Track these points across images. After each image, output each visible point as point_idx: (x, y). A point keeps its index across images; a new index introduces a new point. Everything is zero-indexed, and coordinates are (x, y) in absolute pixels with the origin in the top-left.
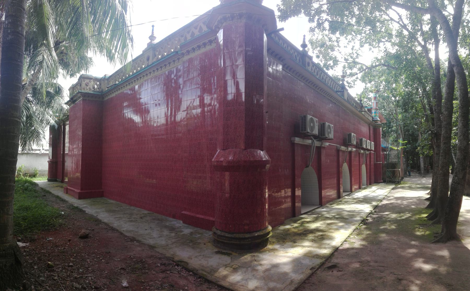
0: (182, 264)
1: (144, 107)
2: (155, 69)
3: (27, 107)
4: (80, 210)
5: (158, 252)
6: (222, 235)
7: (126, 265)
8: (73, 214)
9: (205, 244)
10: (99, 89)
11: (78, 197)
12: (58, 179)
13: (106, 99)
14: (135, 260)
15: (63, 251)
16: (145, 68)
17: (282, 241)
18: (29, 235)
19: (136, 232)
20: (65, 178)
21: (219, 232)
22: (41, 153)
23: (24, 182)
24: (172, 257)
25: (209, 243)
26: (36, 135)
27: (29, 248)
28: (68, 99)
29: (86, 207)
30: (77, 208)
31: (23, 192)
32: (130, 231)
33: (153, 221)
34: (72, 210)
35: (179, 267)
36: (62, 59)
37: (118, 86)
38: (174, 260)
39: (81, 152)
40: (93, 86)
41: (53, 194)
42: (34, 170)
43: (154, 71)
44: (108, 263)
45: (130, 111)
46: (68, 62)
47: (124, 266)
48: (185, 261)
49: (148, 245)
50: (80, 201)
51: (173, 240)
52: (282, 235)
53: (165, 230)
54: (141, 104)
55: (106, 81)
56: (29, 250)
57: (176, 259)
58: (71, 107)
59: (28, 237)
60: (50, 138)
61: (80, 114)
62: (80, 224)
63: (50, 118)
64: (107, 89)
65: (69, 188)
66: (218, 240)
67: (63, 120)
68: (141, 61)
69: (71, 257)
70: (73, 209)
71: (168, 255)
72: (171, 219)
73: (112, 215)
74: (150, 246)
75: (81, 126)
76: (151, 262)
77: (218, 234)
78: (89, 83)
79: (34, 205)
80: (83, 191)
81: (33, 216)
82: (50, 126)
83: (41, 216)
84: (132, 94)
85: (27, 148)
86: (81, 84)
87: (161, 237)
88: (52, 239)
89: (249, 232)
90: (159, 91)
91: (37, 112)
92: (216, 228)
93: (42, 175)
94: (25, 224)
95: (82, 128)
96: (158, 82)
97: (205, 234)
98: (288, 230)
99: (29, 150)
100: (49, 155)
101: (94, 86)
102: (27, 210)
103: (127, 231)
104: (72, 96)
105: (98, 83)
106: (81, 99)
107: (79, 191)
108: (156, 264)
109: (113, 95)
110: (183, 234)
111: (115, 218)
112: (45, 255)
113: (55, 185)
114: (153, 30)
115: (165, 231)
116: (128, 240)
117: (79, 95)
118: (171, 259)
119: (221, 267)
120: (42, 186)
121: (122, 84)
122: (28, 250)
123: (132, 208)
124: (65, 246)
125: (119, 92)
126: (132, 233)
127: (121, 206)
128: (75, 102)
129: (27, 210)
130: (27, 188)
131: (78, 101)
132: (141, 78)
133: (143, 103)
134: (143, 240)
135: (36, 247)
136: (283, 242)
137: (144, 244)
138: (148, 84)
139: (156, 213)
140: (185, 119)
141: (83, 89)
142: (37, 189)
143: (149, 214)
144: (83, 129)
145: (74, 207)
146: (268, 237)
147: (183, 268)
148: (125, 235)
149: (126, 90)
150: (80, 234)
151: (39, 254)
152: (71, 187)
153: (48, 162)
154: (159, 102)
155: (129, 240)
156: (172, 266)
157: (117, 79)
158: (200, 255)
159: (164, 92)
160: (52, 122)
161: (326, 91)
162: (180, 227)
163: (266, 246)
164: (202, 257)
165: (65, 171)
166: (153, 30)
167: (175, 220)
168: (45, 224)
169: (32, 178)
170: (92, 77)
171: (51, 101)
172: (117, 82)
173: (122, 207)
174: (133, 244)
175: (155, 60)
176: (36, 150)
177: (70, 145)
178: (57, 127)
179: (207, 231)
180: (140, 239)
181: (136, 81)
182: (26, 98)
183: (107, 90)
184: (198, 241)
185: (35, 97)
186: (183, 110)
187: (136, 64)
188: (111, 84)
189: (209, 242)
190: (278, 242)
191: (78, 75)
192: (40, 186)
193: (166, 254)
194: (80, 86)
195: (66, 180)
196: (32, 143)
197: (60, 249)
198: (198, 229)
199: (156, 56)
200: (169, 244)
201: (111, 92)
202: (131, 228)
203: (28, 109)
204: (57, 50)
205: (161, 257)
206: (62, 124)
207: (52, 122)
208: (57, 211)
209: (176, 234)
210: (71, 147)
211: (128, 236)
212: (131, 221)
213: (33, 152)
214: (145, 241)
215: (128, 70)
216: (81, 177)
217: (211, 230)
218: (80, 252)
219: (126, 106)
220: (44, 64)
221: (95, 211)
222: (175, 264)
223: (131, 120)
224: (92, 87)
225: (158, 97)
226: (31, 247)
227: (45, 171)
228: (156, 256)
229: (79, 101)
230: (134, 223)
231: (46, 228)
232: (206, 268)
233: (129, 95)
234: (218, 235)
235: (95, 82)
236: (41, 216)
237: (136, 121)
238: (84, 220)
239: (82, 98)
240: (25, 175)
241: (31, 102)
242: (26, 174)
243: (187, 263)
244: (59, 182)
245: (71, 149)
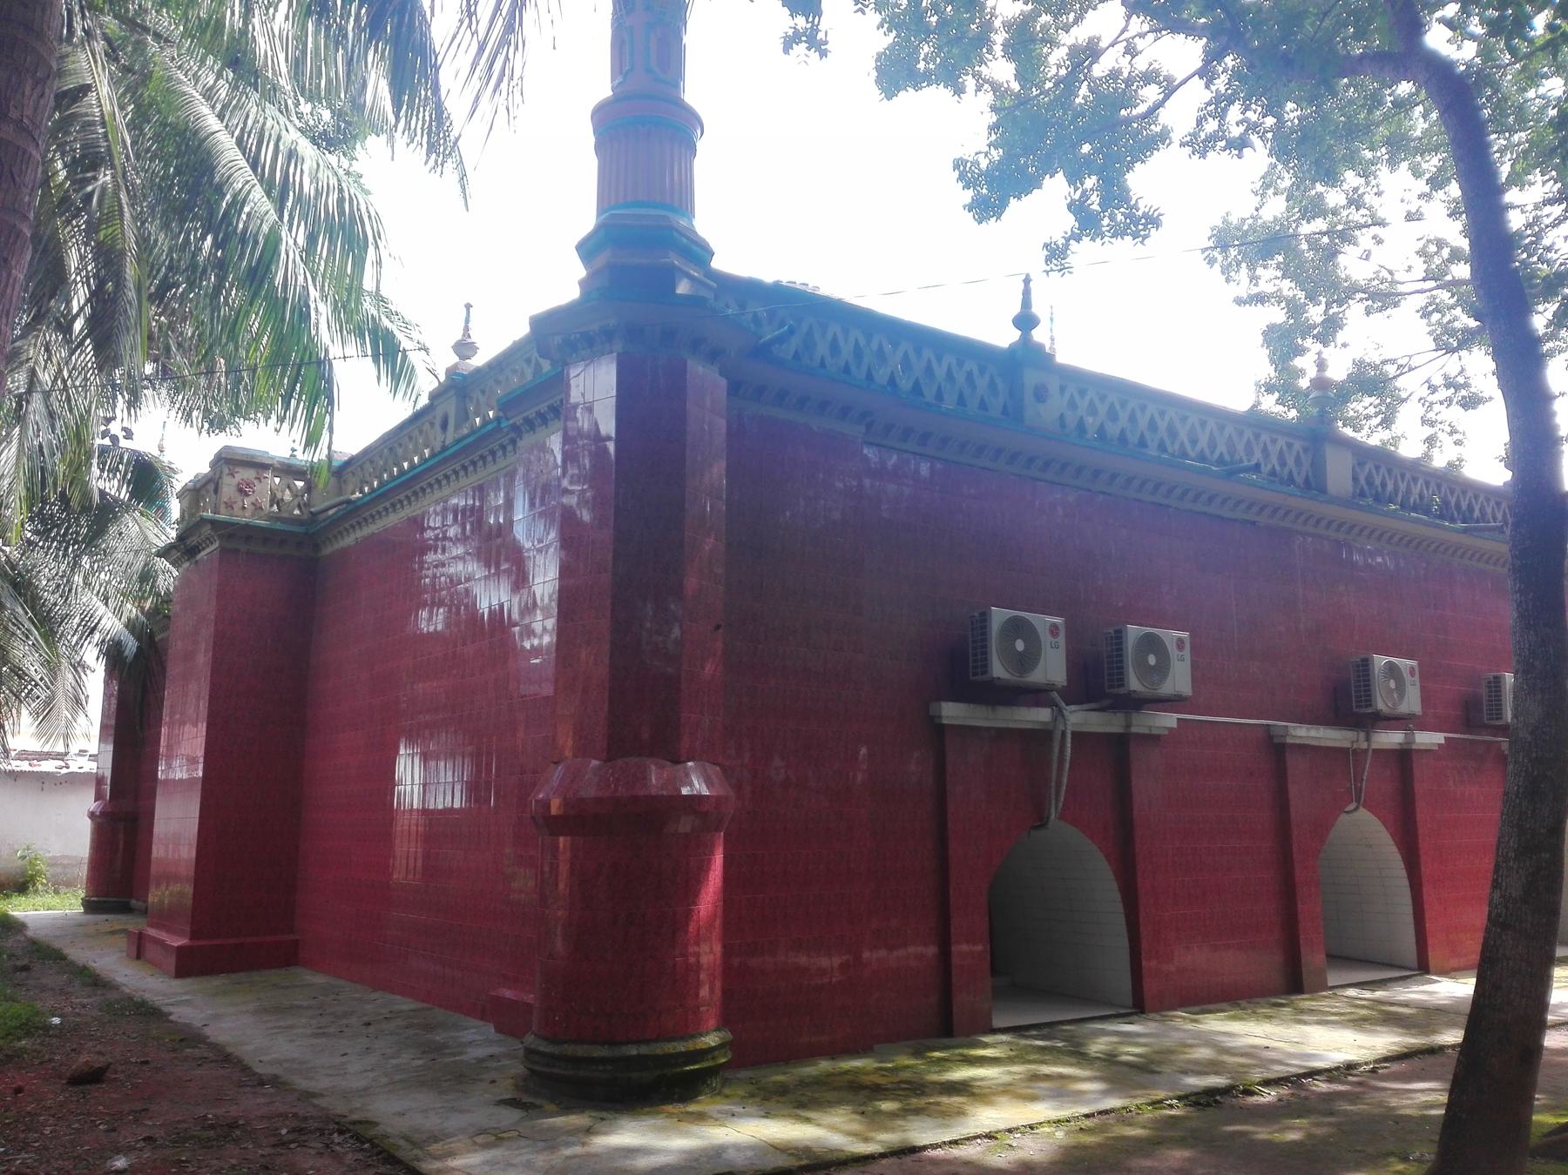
11: (172, 969)
12: (133, 902)
13: (327, 550)
22: (64, 771)
28: (1200, 64)
37: (357, 509)
41: (72, 963)
42: (23, 858)
63: (102, 609)
65: (152, 932)
78: (256, 482)
89: (612, 1043)
93: (59, 885)
109: (349, 540)
114: (467, 321)
128: (196, 554)
141: (223, 506)
153: (92, 815)
161: (1365, 527)
166: (467, 321)
239: (216, 545)
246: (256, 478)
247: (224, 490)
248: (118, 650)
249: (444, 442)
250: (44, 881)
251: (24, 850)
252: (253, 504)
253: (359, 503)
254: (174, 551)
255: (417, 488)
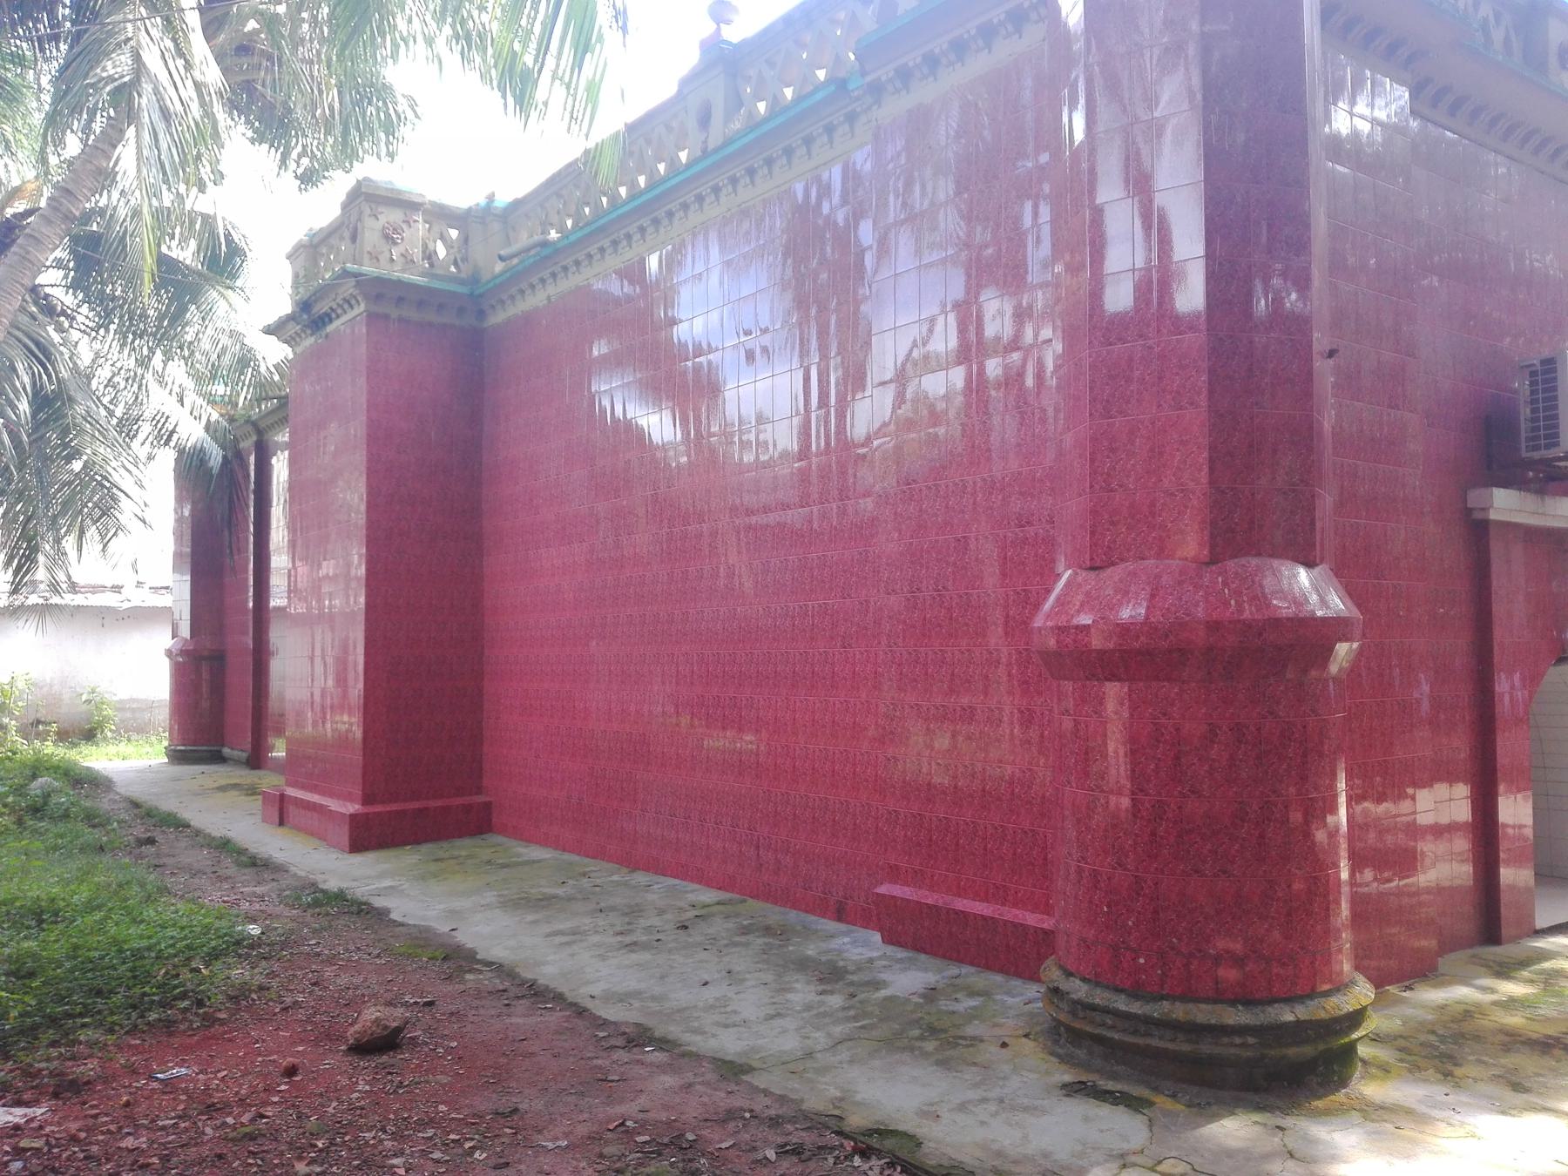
0: (889, 1143)
1: (689, 363)
2: (739, 171)
3: (37, 344)
4: (355, 908)
5: (766, 1092)
6: (1097, 1001)
7: (599, 1167)
8: (315, 931)
9: (1004, 1045)
10: (456, 263)
11: (345, 840)
12: (226, 751)
13: (497, 318)
14: (647, 1138)
15: (247, 1130)
16: (689, 166)
17: (1438, 1070)
18: (48, 1060)
19: (653, 998)
20: (271, 740)
21: (1079, 989)
23: (28, 772)
24: (836, 1112)
25: (1024, 1039)
26: (96, 505)
27: (48, 1129)
28: (286, 308)
29: (391, 887)
30: (340, 896)
31: (20, 822)
32: (624, 998)
33: (743, 939)
34: (310, 911)
35: (875, 1162)
36: (248, 81)
38: (847, 1129)
39: (362, 600)
40: (425, 246)
41: (198, 833)
42: (88, 701)
43: (734, 181)
44: (507, 1164)
45: (622, 386)
46: (285, 103)
47: (591, 1170)
48: (901, 1128)
49: (714, 1060)
50: (357, 859)
51: (838, 1030)
52: (1432, 1038)
53: (797, 981)
54: (678, 353)
55: (496, 226)
56: (47, 1143)
57: (856, 1121)
58: (299, 350)
59: (41, 1070)
60: (179, 520)
61: (354, 392)
62: (357, 980)
64: (499, 267)
65: (291, 792)
66: (1077, 1025)
67: (254, 424)
68: (669, 128)
69: (300, 1158)
70: (316, 903)
71: (814, 1103)
72: (831, 925)
73: (535, 922)
74: (725, 1062)
75: (360, 458)
76: (723, 1146)
77: (1074, 996)
79: (83, 894)
80: (379, 808)
81: (75, 958)
82: (181, 451)
83: (121, 951)
84: (629, 299)
85: (41, 574)
86: (356, 229)
87: (778, 1015)
88: (184, 1071)
89: (1249, 1002)
90: (763, 284)
91: (104, 373)
92: (1061, 967)
93: (133, 728)
94: (26, 999)
95: (363, 469)
96: (758, 238)
97: (1006, 998)
98: (1469, 1013)
99: (54, 587)
100: (177, 616)
101: (431, 246)
102: (41, 922)
103: (610, 997)
104: (304, 293)
105: (454, 233)
106: (356, 311)
107: (353, 808)
108: (754, 1149)
110: (886, 999)
111: (548, 935)
112: (142, 1160)
113: (210, 783)
115: (798, 986)
116: (613, 1042)
117: (348, 288)
118: (831, 1123)
119: (1098, 1164)
120: (136, 792)
121: (580, 241)
122: (37, 1144)
123: (641, 878)
124: (266, 1103)
125: (566, 284)
126: (637, 1004)
127: (584, 875)
128: (324, 325)
129: (41, 922)
130: (46, 804)
131: (344, 318)
132: (670, 214)
133: (686, 344)
134: (687, 1037)
135: (91, 1122)
136: (1446, 1075)
137: (697, 1057)
138: (707, 248)
139: (755, 896)
140: (892, 427)
141: (366, 257)
142: (104, 804)
143: (721, 908)
144: (371, 473)
145: (324, 892)
146: (1355, 1036)
147: (891, 1165)
148: (600, 1017)
149: (604, 278)
150: (352, 1030)
151: (108, 1160)
152: (303, 787)
153: (169, 653)
154: (766, 340)
155: (620, 1042)
156: (837, 1158)
157: (555, 219)
158: (984, 1100)
159: (783, 290)
160: (192, 432)
162: (871, 961)
163: (1343, 1082)
164: (994, 1108)
165: (273, 704)
167: (842, 927)
168: (144, 994)
169: (74, 745)
170: (419, 200)
171: (183, 310)
172: (554, 235)
173: (586, 880)
174: (640, 1062)
175: (736, 125)
176: (96, 589)
177: (298, 563)
178: (220, 459)
179: (1016, 983)
180: (673, 1031)
181: (650, 230)
182: (34, 290)
183: (503, 272)
184: (970, 1030)
185: (86, 290)
186: (876, 381)
187: (649, 142)
188: (524, 239)
189: (1026, 1036)
190: (1410, 1071)
191: (338, 186)
192: (122, 791)
193: (802, 1101)
194: (354, 238)
195: (279, 752)
196: (69, 543)
197: (230, 1120)
198: (966, 969)
199: (741, 104)
200: (819, 1047)
201: (524, 285)
202: (632, 983)
203: (42, 354)
204: (219, 29)
205: (778, 1116)
206: (247, 444)
207: (192, 432)
208: (217, 924)
209: (853, 996)
210: (302, 569)
211: (615, 1023)
212: (633, 946)
213: (79, 600)
214: (698, 1038)
215: (605, 169)
216: (365, 732)
217: (1034, 977)
218: (350, 1123)
219: (604, 359)
220: (144, 101)
221: (442, 906)
222: (849, 1145)
223: (633, 435)
224: (417, 253)
225: (756, 315)
226: (59, 1124)
227: (151, 706)
228: (751, 1111)
229: (349, 322)
230: (644, 956)
231: (153, 1016)
232: (1015, 1162)
233: (617, 302)
234: (1078, 1002)
235: (436, 228)
236: (121, 951)
237: (656, 438)
238: (378, 956)
239: (362, 307)
240: (34, 728)
241: (63, 313)
242: (39, 722)
243: (915, 1142)
244: (237, 762)
245: (302, 583)
246: (404, 221)
247: (367, 234)
248: (201, 460)
249: (705, 142)
250: (113, 727)
251: (89, 693)
252: (402, 255)
253: (560, 245)
254: (292, 324)
255: (661, 213)
